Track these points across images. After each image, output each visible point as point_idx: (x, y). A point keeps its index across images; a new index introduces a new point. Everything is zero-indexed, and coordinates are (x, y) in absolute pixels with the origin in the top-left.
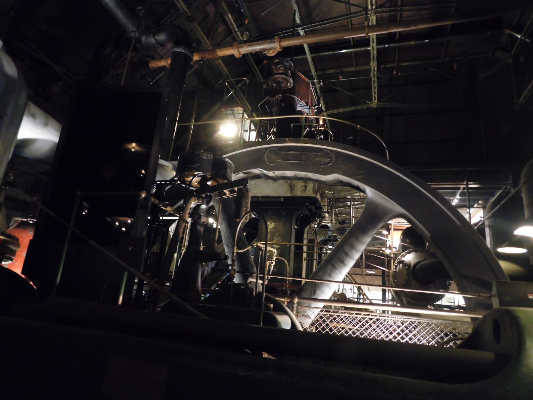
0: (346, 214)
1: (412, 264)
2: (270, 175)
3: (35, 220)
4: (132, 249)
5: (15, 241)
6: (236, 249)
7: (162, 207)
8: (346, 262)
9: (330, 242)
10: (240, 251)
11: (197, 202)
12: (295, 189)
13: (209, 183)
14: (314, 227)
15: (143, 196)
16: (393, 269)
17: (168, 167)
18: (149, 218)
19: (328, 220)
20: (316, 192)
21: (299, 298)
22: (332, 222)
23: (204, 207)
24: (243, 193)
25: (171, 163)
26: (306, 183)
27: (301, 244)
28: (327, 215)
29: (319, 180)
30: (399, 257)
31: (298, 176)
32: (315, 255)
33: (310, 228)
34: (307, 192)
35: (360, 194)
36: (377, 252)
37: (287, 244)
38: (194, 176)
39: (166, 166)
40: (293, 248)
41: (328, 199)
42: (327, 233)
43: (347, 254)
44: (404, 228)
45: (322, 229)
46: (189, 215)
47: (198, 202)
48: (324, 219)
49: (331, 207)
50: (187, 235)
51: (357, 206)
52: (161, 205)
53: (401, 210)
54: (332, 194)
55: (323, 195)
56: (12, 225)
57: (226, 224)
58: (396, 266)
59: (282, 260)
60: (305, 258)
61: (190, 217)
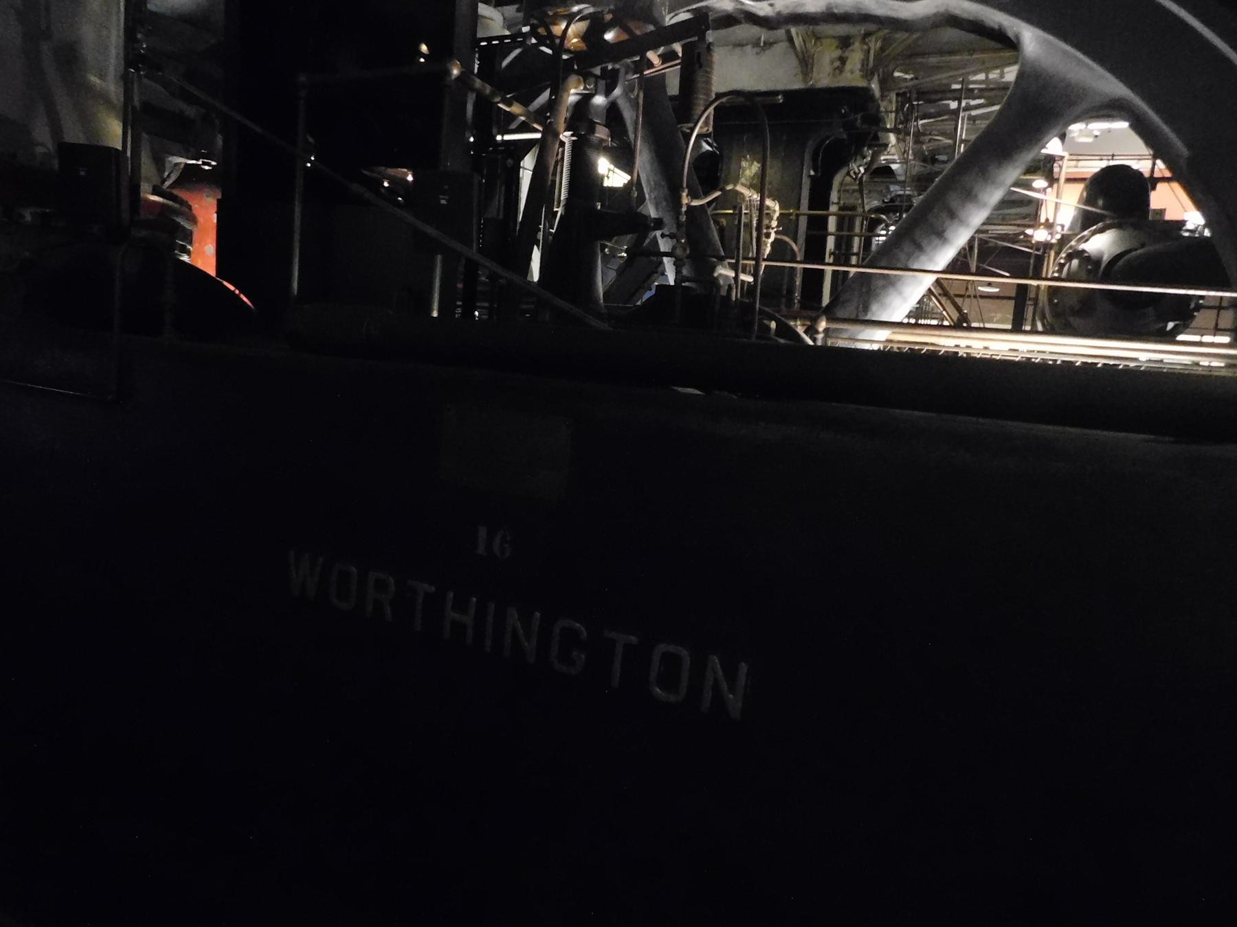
0: (943, 134)
1: (1106, 258)
2: (761, 13)
3: (214, 163)
4: (447, 201)
5: (184, 209)
6: (687, 196)
7: (500, 105)
8: (948, 234)
9: (894, 214)
10: (695, 203)
11: (582, 88)
12: (814, 69)
13: (609, 36)
14: (857, 171)
15: (455, 72)
16: (1053, 272)
17: (490, 21)
18: (472, 139)
19: (894, 154)
20: (868, 73)
21: (829, 320)
22: (905, 155)
23: (599, 100)
24: (699, 55)
25: (499, 11)
26: (845, 51)
27: (825, 212)
28: (892, 138)
29: (894, 18)
30: (1073, 243)
31: (836, 11)
32: (856, 240)
33: (848, 174)
34: (847, 75)
35: (987, 77)
36: (1014, 238)
37: (791, 214)
38: (570, 18)
39: (489, 19)
40: (803, 222)
41: (898, 95)
42: (888, 188)
43: (953, 215)
44: (1089, 176)
45: (876, 180)
46: (565, 122)
47: (585, 88)
48: (885, 149)
49: (905, 119)
50: (564, 175)
51: (974, 113)
52: (498, 99)
53: (1114, 87)
54: (912, 79)
55: (887, 82)
56: (169, 176)
57: (651, 151)
58: (1060, 264)
59: (786, 242)
60: (830, 250)
61: (567, 129)
